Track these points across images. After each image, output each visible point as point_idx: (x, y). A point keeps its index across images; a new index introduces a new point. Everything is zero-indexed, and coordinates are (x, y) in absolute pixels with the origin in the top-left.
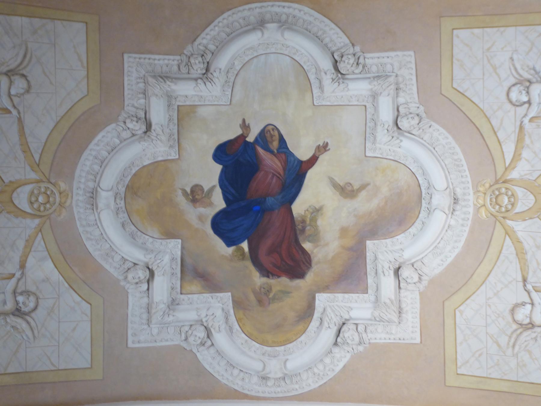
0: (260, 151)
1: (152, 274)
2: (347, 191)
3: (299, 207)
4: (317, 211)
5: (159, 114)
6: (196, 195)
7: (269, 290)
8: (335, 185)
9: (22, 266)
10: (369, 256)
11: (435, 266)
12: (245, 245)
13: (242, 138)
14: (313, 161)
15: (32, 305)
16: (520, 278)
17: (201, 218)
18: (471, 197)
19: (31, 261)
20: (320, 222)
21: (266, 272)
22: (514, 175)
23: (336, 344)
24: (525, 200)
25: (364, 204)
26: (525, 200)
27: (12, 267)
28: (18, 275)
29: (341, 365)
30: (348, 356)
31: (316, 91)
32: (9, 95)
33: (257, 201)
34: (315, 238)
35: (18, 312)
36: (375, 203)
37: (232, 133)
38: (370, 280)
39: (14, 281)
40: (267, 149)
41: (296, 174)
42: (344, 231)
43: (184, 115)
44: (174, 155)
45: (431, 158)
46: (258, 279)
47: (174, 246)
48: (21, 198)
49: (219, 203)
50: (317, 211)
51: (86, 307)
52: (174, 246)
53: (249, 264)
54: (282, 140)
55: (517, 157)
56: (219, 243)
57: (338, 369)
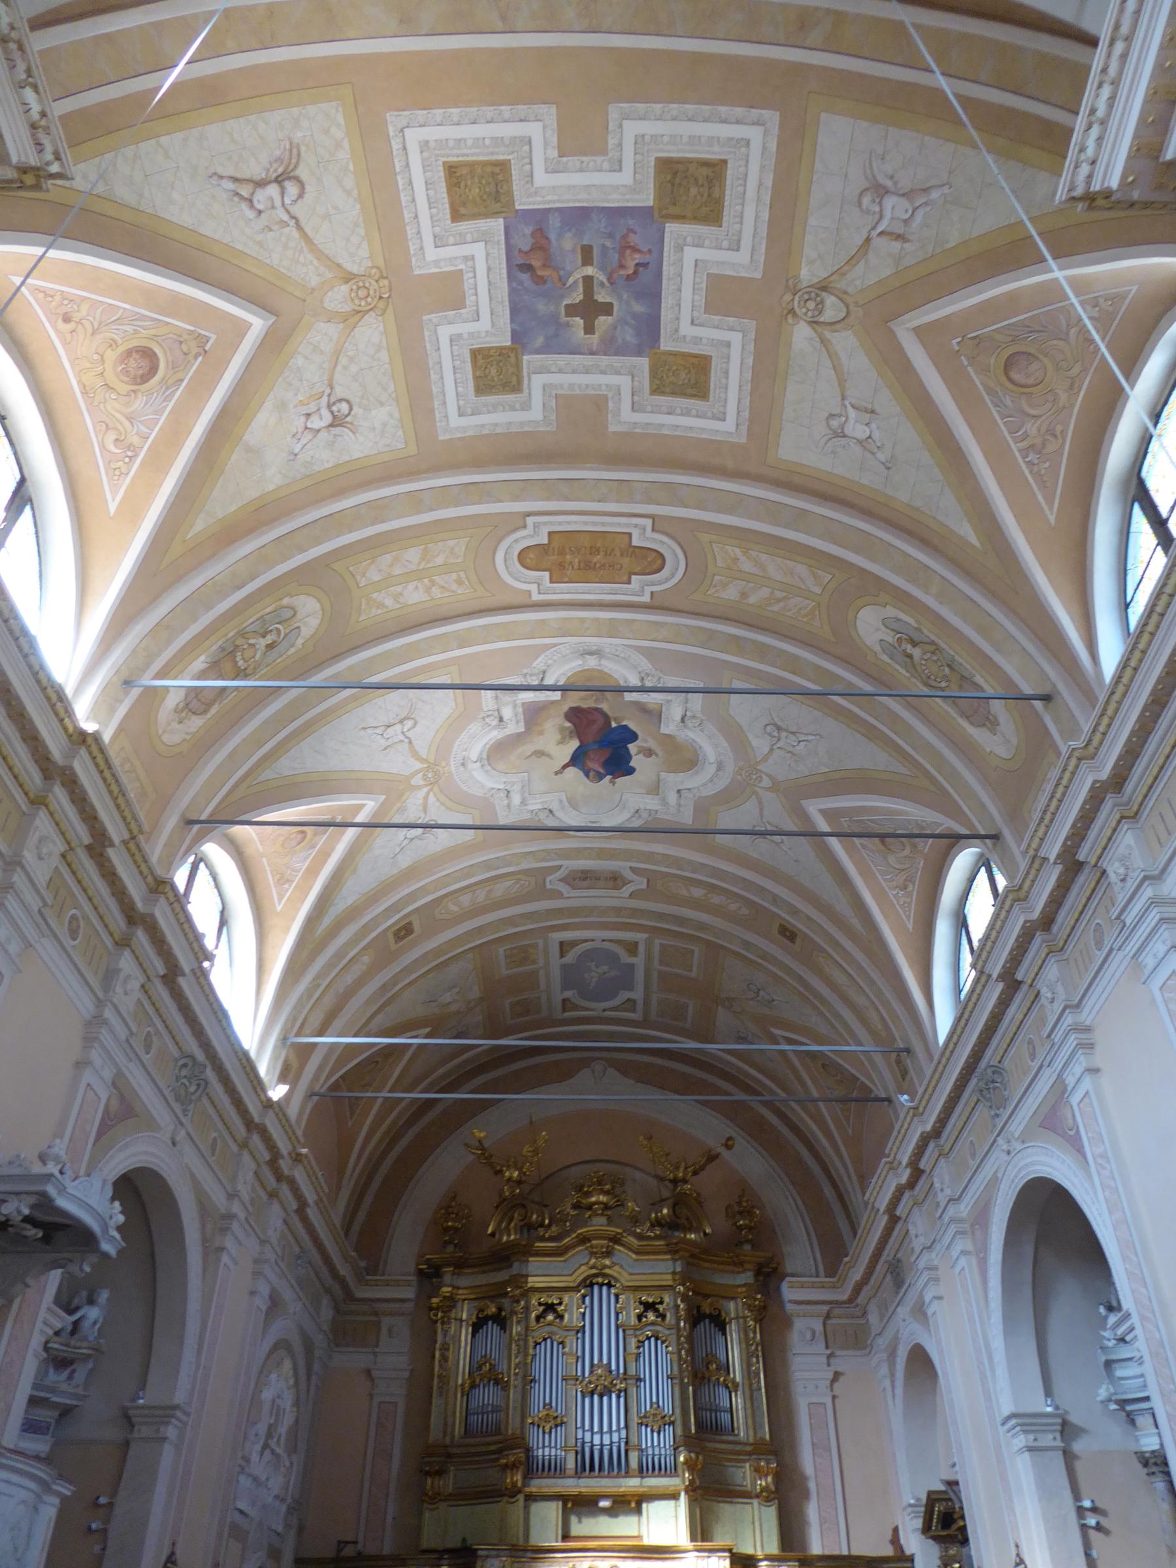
0: (602, 771)
1: (683, 720)
2: (540, 754)
3: (575, 744)
4: (562, 742)
5: (672, 798)
6: (649, 753)
7: (595, 701)
8: (549, 756)
9: (772, 750)
10: (522, 724)
11: (474, 727)
12: (614, 725)
13: (615, 778)
14: (565, 767)
15: (768, 728)
16: (414, 742)
17: (646, 741)
18: (453, 769)
19: (766, 750)
20: (559, 737)
21: (600, 711)
22: (426, 790)
23: (544, 672)
24: (417, 780)
25: (528, 748)
26: (417, 780)
27: (777, 753)
28: (874, 233)
29: (540, 659)
30: (534, 665)
31: (565, 799)
32: (847, 417)
33: (603, 744)
34: (562, 729)
35: (779, 729)
36: (520, 750)
37: (621, 781)
38: (520, 710)
39: (879, 229)
40: (598, 773)
41: (576, 760)
42: (541, 733)
43: (655, 789)
44: (663, 775)
45: (483, 781)
46: (604, 706)
47: (664, 730)
48: (766, 783)
49: (632, 748)
50: (562, 742)
51: (732, 713)
52: (664, 730)
53: (609, 713)
54: (587, 776)
55: (426, 798)
56: (632, 726)
57: (542, 656)
